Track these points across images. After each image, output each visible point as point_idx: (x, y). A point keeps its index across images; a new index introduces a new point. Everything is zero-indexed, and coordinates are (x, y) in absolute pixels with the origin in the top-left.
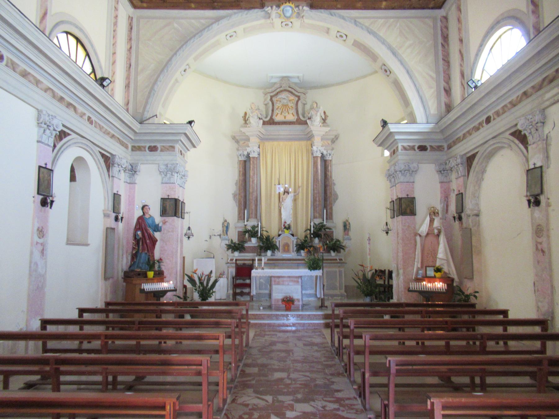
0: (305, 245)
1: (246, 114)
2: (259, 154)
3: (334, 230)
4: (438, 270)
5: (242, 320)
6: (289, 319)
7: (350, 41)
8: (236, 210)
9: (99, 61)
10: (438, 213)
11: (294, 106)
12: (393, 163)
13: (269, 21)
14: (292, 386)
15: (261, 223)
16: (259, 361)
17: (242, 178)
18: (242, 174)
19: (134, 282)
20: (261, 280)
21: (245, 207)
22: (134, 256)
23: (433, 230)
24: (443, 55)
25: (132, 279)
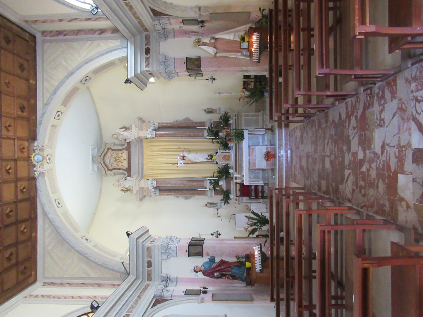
0: (224, 143)
1: (122, 190)
2: (154, 179)
3: (213, 121)
4: (243, 39)
5: (284, 193)
6: (282, 155)
7: (62, 109)
8: (197, 197)
9: (78, 310)
10: (198, 39)
11: (116, 152)
12: (159, 75)
13: (46, 173)
14: (337, 154)
15: (208, 178)
16: (316, 179)
17: (173, 193)
18: (169, 192)
19: (255, 277)
20: (252, 177)
21: (195, 190)
22: (234, 277)
23: (212, 43)
24: (73, 35)
25: (252, 279)
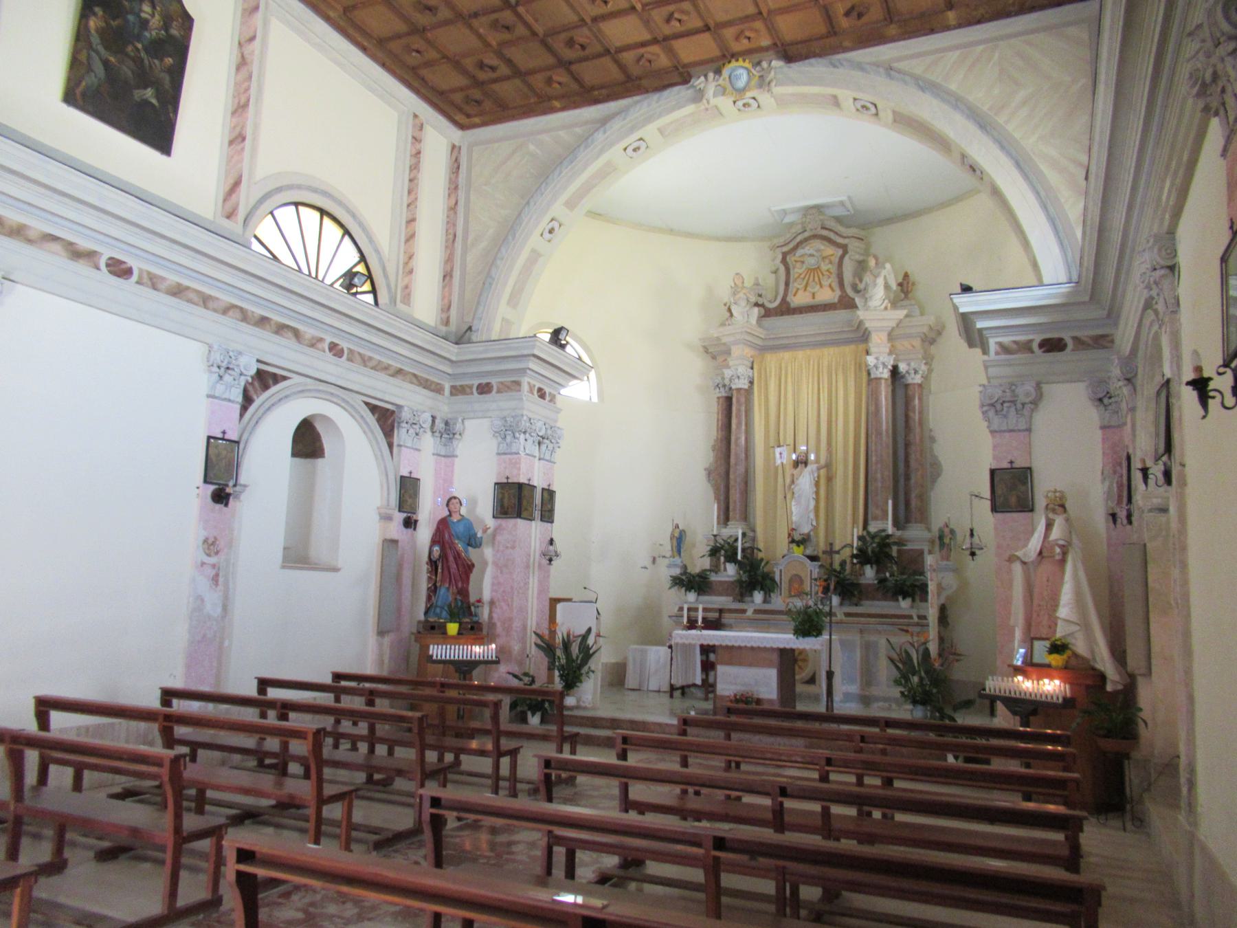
2: (751, 383)
7: (887, 115)
11: (834, 269)
23: (1052, 548)
